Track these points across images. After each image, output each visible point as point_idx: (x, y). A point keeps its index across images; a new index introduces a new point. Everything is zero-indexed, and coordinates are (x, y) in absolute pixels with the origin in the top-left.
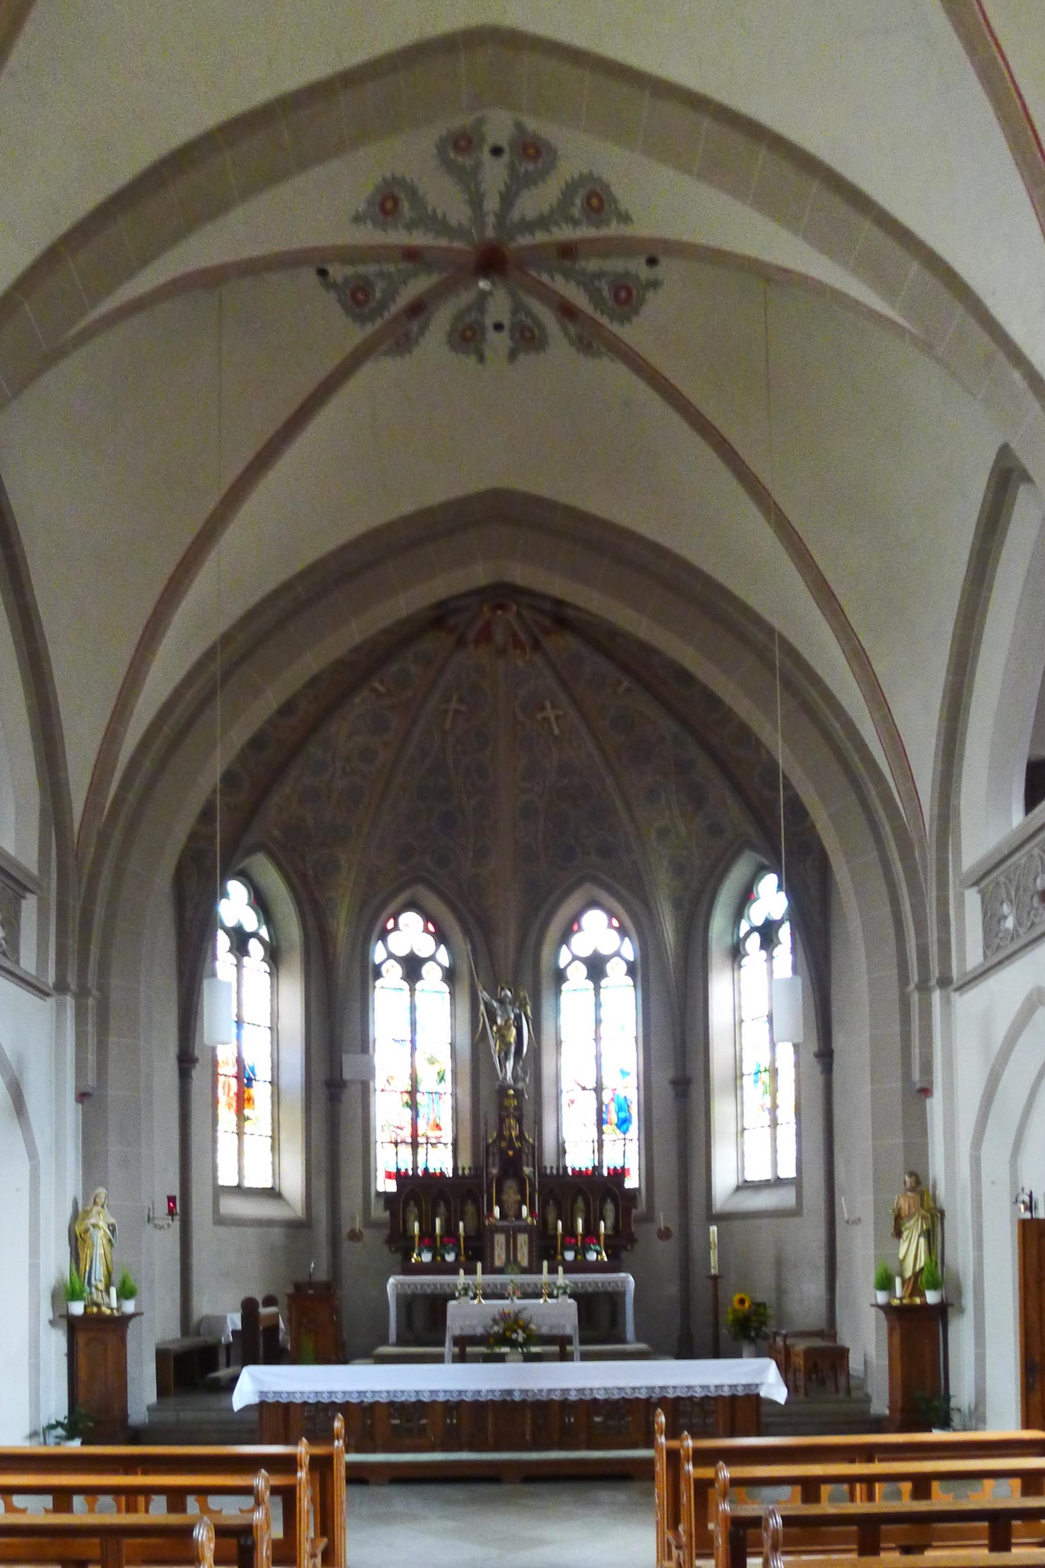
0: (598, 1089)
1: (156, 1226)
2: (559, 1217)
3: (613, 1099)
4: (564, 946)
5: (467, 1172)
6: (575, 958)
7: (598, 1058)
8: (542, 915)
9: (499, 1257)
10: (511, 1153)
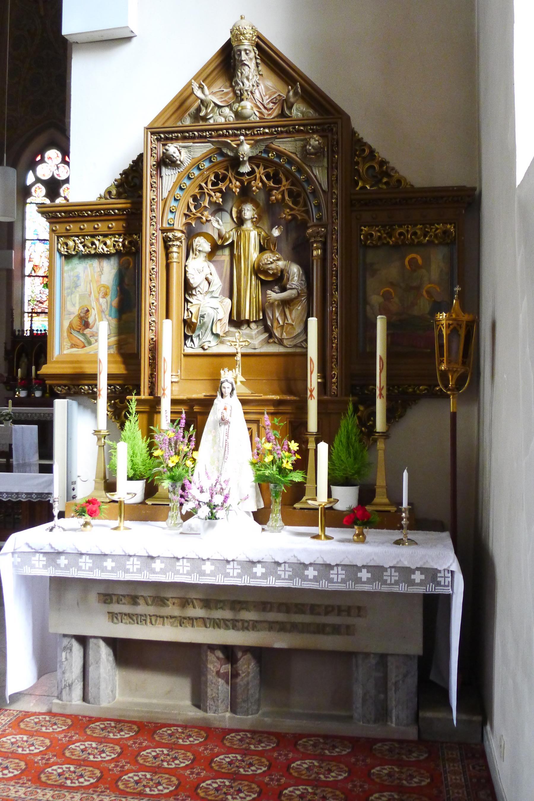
4: (31, 172)
6: (38, 180)
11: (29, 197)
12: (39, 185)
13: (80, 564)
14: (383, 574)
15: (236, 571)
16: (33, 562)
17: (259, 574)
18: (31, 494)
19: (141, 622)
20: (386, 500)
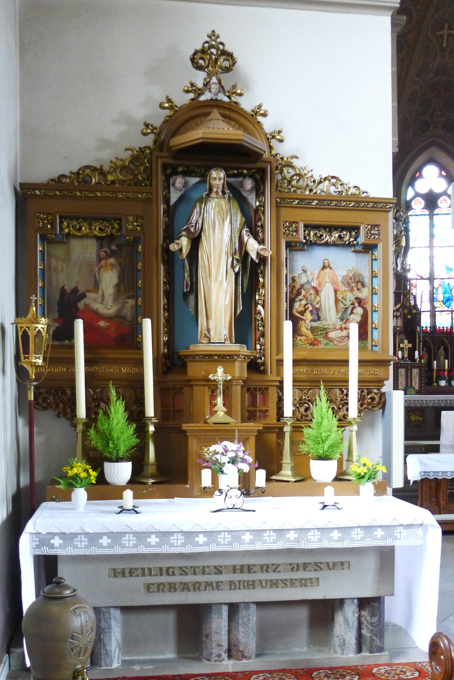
0: (431, 279)
1: (322, 419)
2: (446, 358)
3: (440, 285)
4: (410, 188)
5: (429, 329)
6: (417, 195)
7: (431, 259)
8: (409, 157)
9: (401, 383)
10: (409, 317)
11: (410, 210)
12: (419, 199)
13: (309, 537)
14: (170, 538)
15: (83, 544)
16: (219, 540)
17: (379, 536)
18: (446, 472)
19: (248, 586)
20: (290, 473)
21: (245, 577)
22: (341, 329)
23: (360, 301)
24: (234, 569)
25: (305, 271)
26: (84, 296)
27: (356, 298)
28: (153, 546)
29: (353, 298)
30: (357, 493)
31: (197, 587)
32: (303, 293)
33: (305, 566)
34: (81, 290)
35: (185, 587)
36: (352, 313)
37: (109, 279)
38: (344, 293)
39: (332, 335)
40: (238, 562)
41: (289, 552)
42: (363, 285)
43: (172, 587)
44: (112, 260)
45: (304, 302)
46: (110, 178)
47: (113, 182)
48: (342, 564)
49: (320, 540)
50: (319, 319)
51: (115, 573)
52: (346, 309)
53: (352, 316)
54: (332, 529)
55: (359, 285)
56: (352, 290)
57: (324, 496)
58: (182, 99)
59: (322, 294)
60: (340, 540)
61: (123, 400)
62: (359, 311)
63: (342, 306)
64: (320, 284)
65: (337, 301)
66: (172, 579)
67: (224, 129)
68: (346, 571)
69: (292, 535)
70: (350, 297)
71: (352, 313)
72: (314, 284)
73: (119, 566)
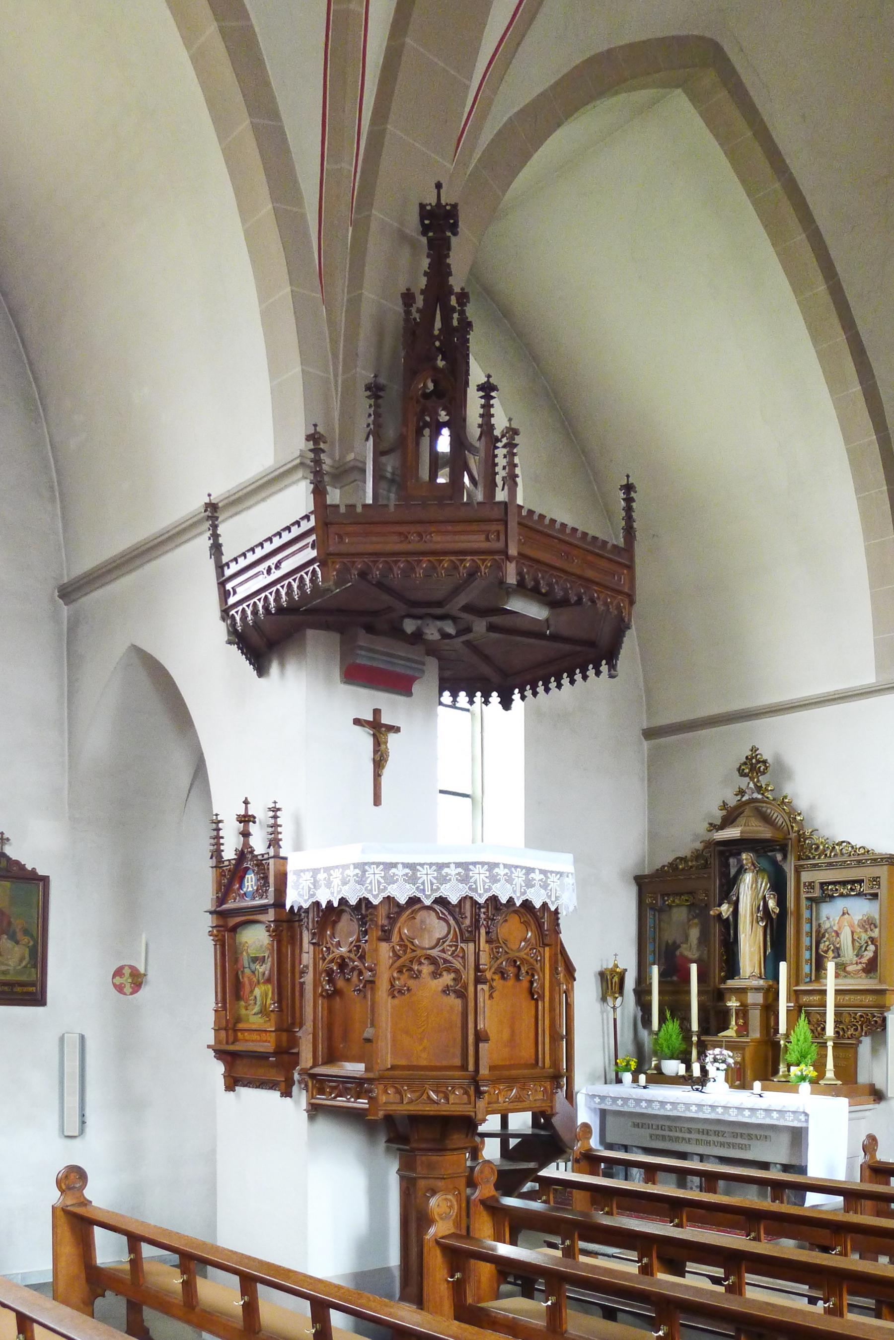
21: (704, 1137)
22: (857, 963)
23: (872, 940)
24: (698, 1131)
25: (828, 918)
26: (679, 947)
27: (870, 938)
28: (656, 1110)
29: (866, 938)
30: (797, 1092)
31: (677, 1139)
32: (827, 935)
33: (742, 1135)
34: (678, 942)
35: (671, 1139)
36: (866, 950)
37: (694, 934)
38: (529, 978)
39: (849, 969)
40: (700, 1126)
41: (719, 1122)
42: (876, 927)
43: (664, 1138)
44: (696, 921)
45: (827, 943)
46: (690, 864)
47: (691, 867)
48: (766, 1137)
49: (736, 1116)
50: (839, 956)
51: (636, 1125)
52: (861, 947)
53: (866, 953)
54: (744, 1109)
55: (872, 926)
56: (866, 931)
57: (797, 1092)
58: (732, 801)
59: (842, 936)
60: (750, 1117)
61: (673, 1019)
62: (872, 948)
63: (857, 944)
64: (840, 928)
65: (853, 940)
66: (663, 1133)
67: (343, 964)
68: (768, 1143)
69: (720, 1110)
70: (864, 937)
71: (866, 950)
72: (835, 928)
73: (637, 1121)
